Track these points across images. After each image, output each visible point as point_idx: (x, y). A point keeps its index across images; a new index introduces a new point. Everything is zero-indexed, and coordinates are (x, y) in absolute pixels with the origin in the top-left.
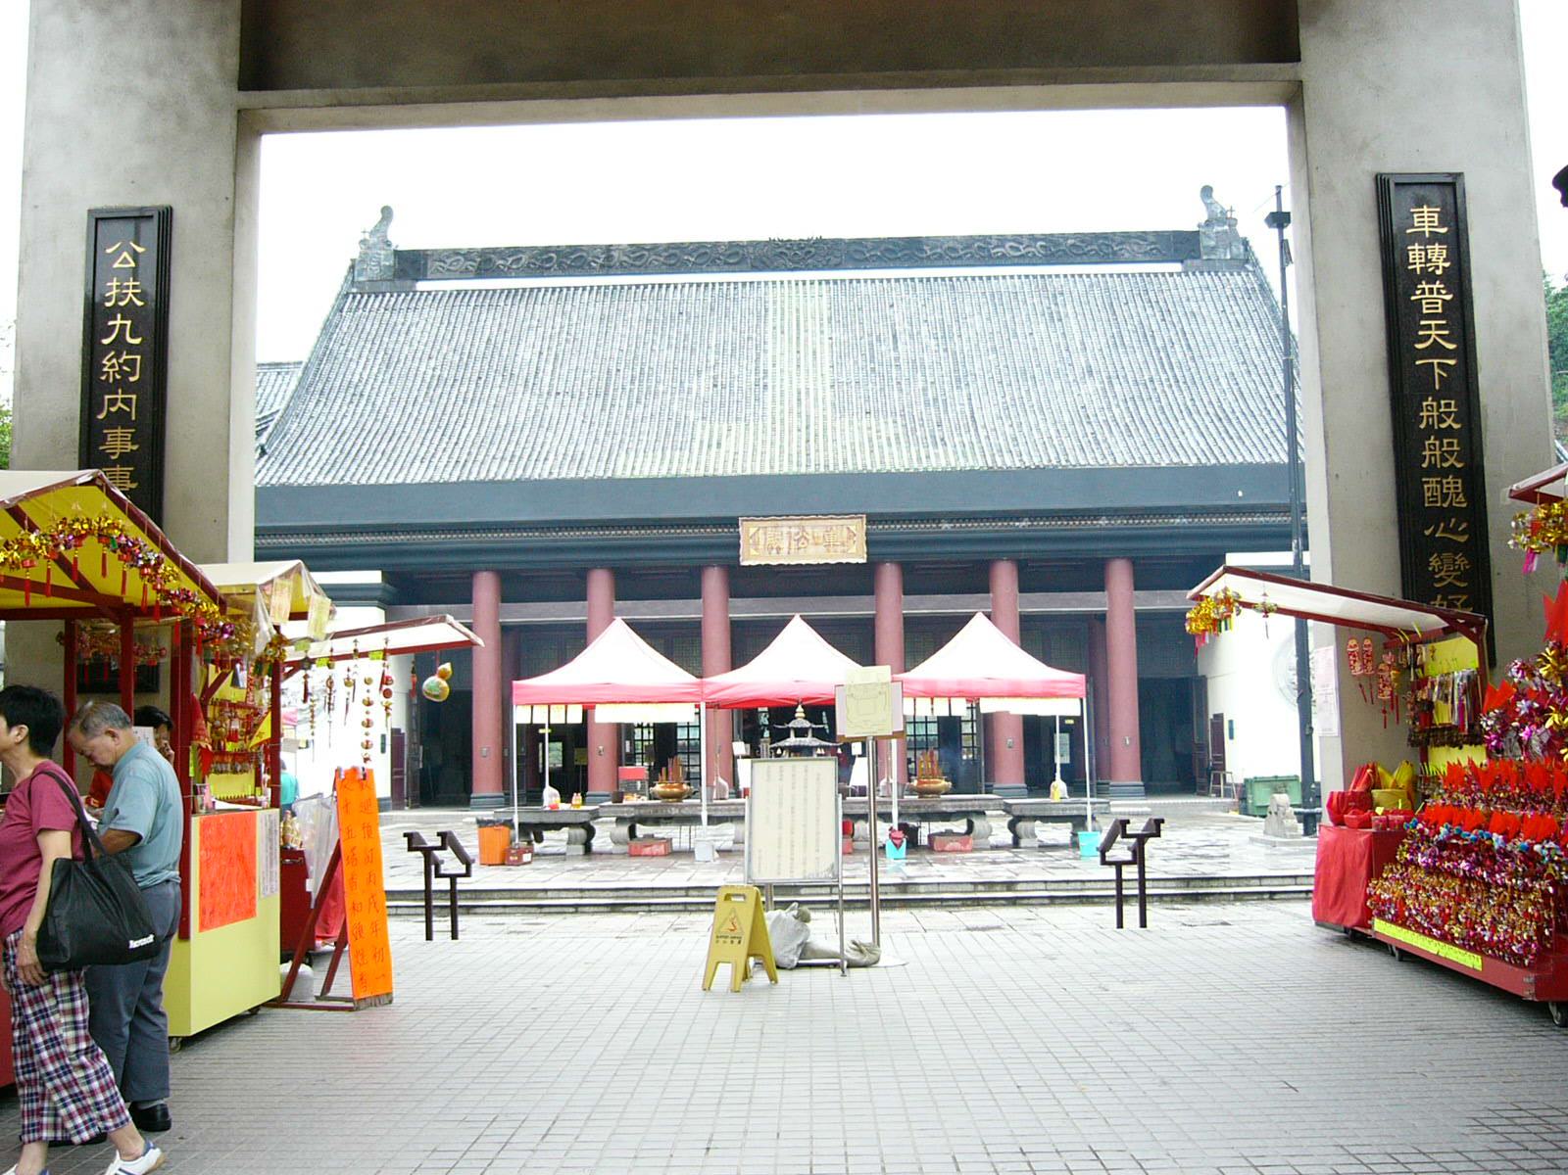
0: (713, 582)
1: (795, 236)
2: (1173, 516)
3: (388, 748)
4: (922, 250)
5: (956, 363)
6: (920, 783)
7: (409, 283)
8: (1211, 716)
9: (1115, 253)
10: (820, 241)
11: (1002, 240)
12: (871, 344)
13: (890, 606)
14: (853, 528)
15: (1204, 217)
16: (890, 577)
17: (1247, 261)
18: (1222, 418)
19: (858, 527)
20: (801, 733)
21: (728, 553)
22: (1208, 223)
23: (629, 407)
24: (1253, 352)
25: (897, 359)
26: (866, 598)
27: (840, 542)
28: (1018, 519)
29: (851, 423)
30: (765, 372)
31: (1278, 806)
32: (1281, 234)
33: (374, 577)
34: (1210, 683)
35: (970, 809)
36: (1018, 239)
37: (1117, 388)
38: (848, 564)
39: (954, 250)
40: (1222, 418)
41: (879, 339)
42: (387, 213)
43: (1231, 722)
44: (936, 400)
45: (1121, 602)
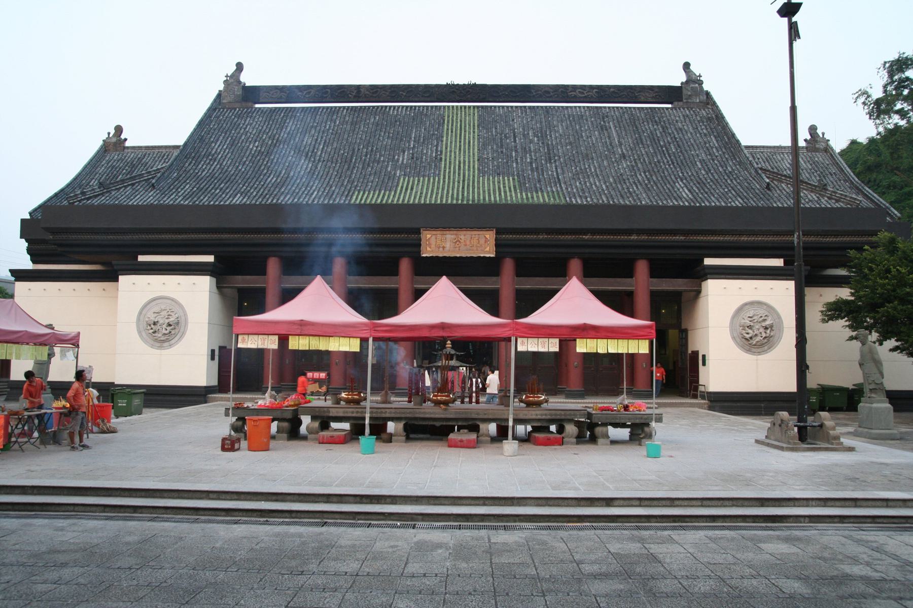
0: (405, 266)
1: (461, 83)
2: (675, 235)
3: (217, 358)
4: (530, 92)
5: (548, 149)
6: (527, 397)
7: (250, 104)
8: (690, 352)
9: (636, 97)
10: (475, 85)
11: (574, 87)
12: (501, 139)
13: (507, 283)
14: (488, 236)
15: (684, 79)
16: (508, 266)
17: (708, 104)
18: (701, 183)
19: (490, 236)
20: (450, 357)
21: (414, 249)
22: (687, 82)
23: (363, 168)
24: (714, 150)
25: (516, 147)
26: (494, 279)
27: (481, 244)
28: (585, 234)
29: (489, 179)
30: (441, 152)
31: (782, 420)
32: (790, 20)
33: (210, 259)
34: (690, 333)
35: (563, 417)
36: (583, 87)
37: (640, 165)
38: (484, 257)
39: (548, 92)
40: (701, 183)
41: (505, 136)
42: (240, 67)
43: (704, 356)
44: (537, 168)
45: (642, 282)
